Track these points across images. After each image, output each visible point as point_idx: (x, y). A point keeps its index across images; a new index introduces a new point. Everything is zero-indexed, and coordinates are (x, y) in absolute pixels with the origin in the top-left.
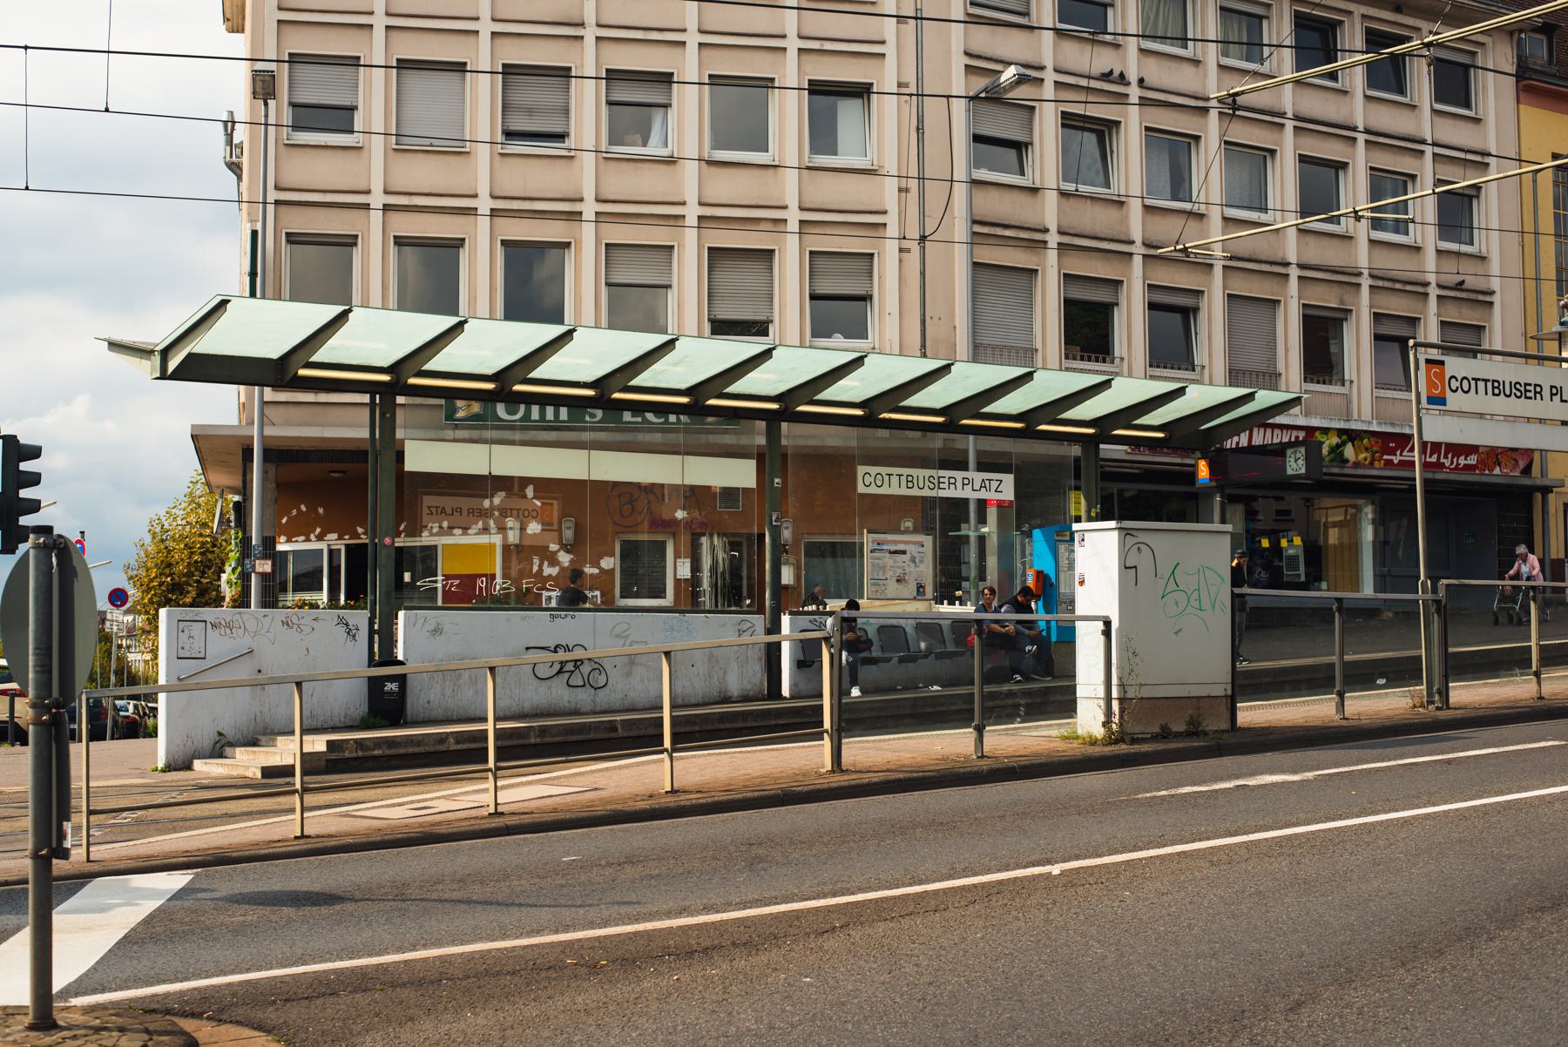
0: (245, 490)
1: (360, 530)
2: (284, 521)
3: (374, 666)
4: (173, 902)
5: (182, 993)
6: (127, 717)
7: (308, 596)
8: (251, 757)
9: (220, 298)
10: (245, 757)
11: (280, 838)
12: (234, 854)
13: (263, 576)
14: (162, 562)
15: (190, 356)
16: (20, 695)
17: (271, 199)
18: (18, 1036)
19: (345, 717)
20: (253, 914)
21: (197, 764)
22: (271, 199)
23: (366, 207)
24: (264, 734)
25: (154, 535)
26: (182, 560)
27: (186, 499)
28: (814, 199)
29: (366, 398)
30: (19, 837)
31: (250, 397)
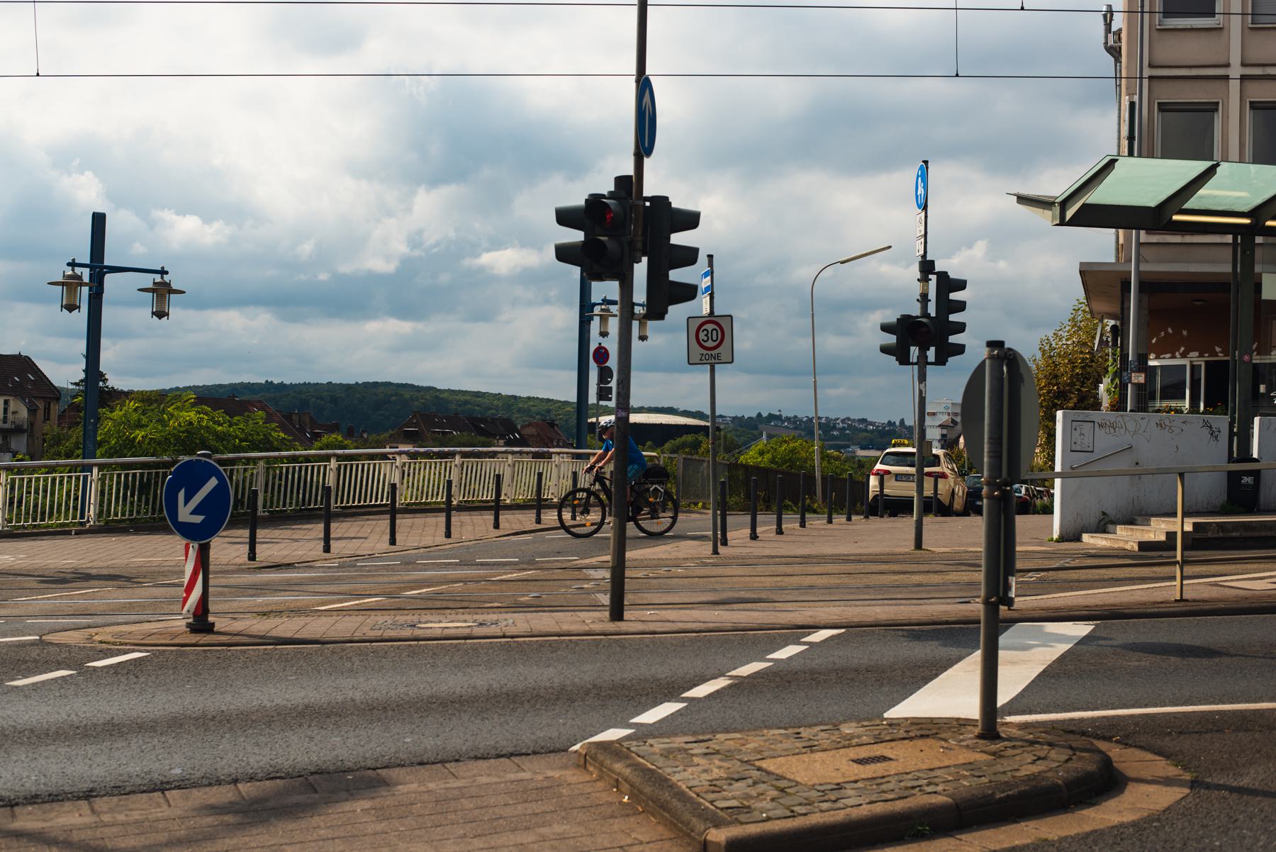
0: (1123, 317)
1: (1218, 349)
2: (1154, 341)
3: (1234, 462)
4: (1080, 646)
5: (1093, 720)
6: (1020, 497)
7: (1173, 404)
8: (1129, 533)
9: (1108, 158)
10: (1124, 533)
11: (1162, 600)
12: (1126, 611)
13: (1138, 386)
14: (1050, 374)
15: (1084, 205)
16: (941, 477)
17: (1145, 74)
18: (970, 742)
19: (1208, 503)
20: (1147, 660)
21: (1086, 537)
22: (1145, 74)
23: (1227, 78)
24: (1140, 515)
25: (1044, 352)
26: (1066, 372)
27: (1070, 323)
28: (1255, 55)
29: (1229, 239)
30: (950, 587)
31: (1129, 239)
